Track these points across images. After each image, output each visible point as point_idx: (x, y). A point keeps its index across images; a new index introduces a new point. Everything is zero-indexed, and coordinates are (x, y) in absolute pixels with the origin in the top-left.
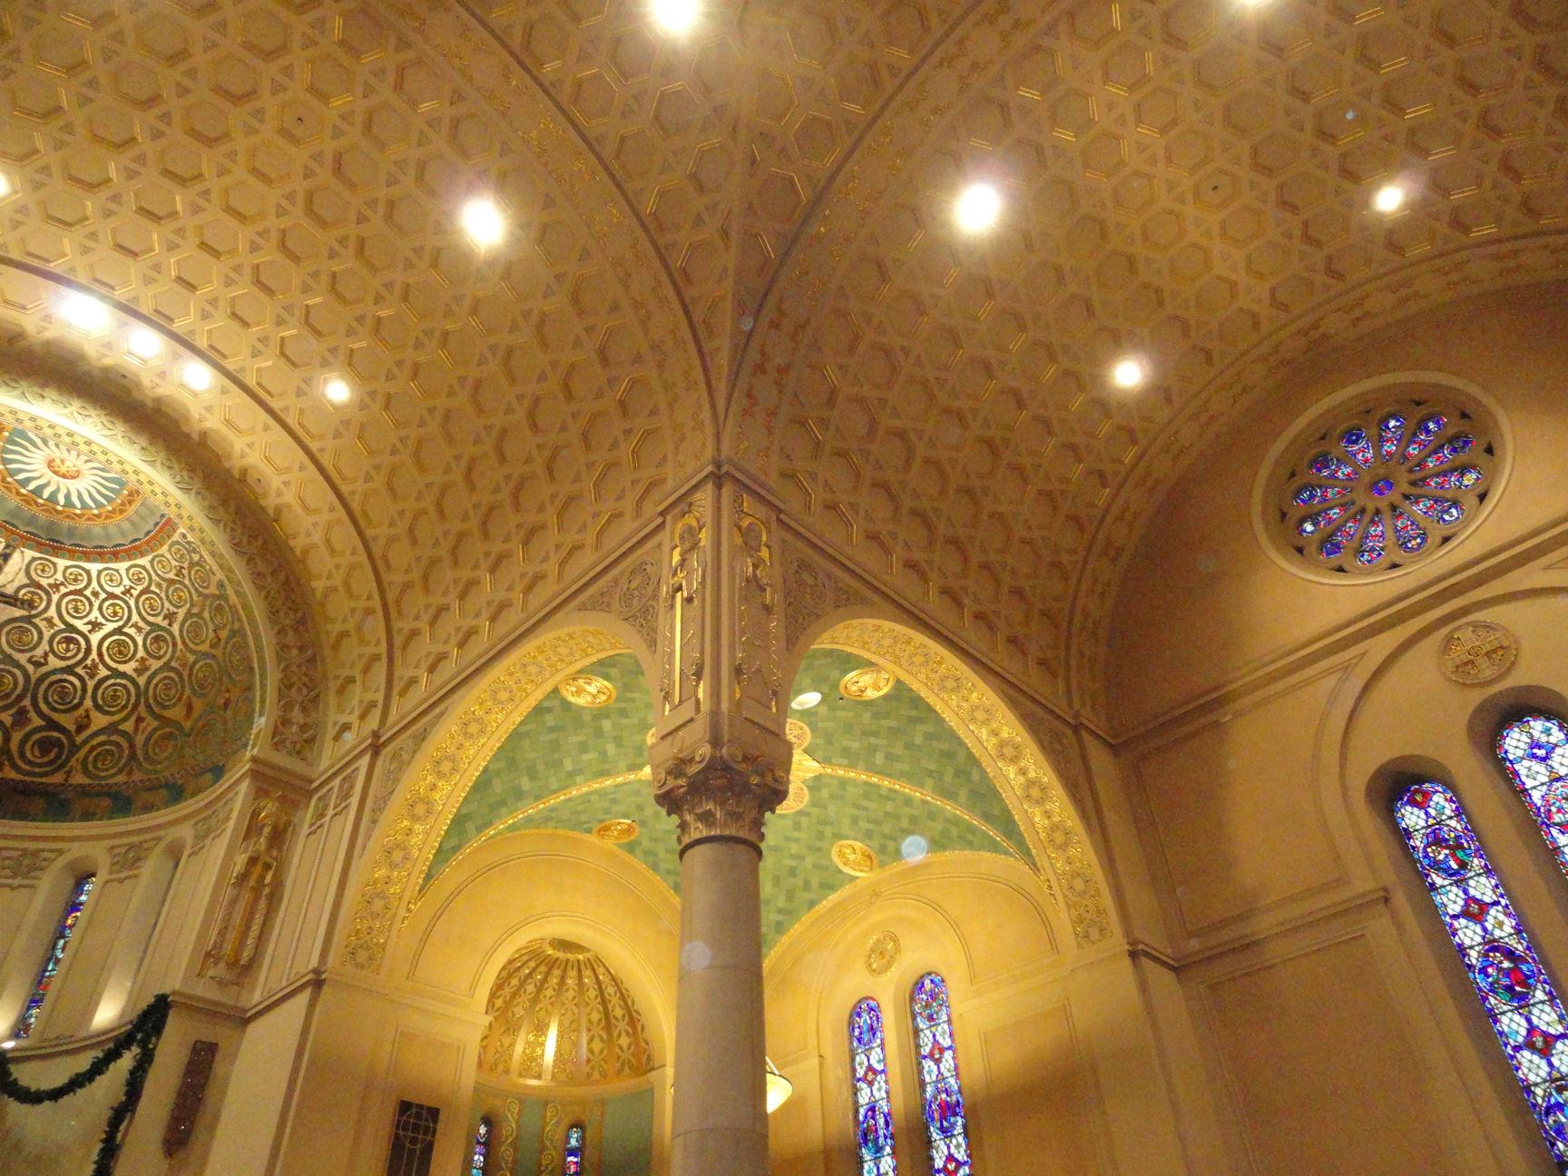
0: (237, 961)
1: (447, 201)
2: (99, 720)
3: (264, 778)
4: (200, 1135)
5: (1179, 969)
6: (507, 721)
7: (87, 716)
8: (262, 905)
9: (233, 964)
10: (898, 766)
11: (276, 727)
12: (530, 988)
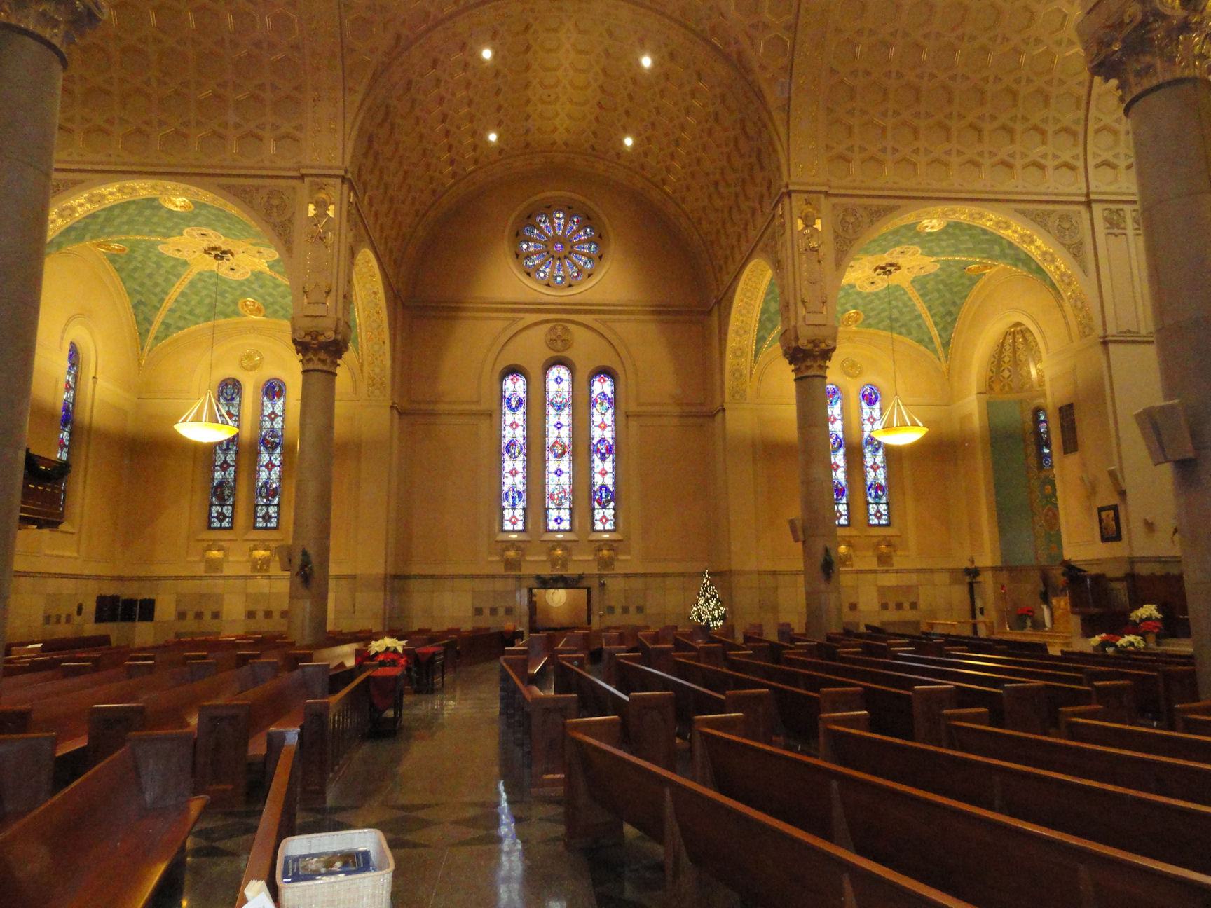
5: (400, 414)
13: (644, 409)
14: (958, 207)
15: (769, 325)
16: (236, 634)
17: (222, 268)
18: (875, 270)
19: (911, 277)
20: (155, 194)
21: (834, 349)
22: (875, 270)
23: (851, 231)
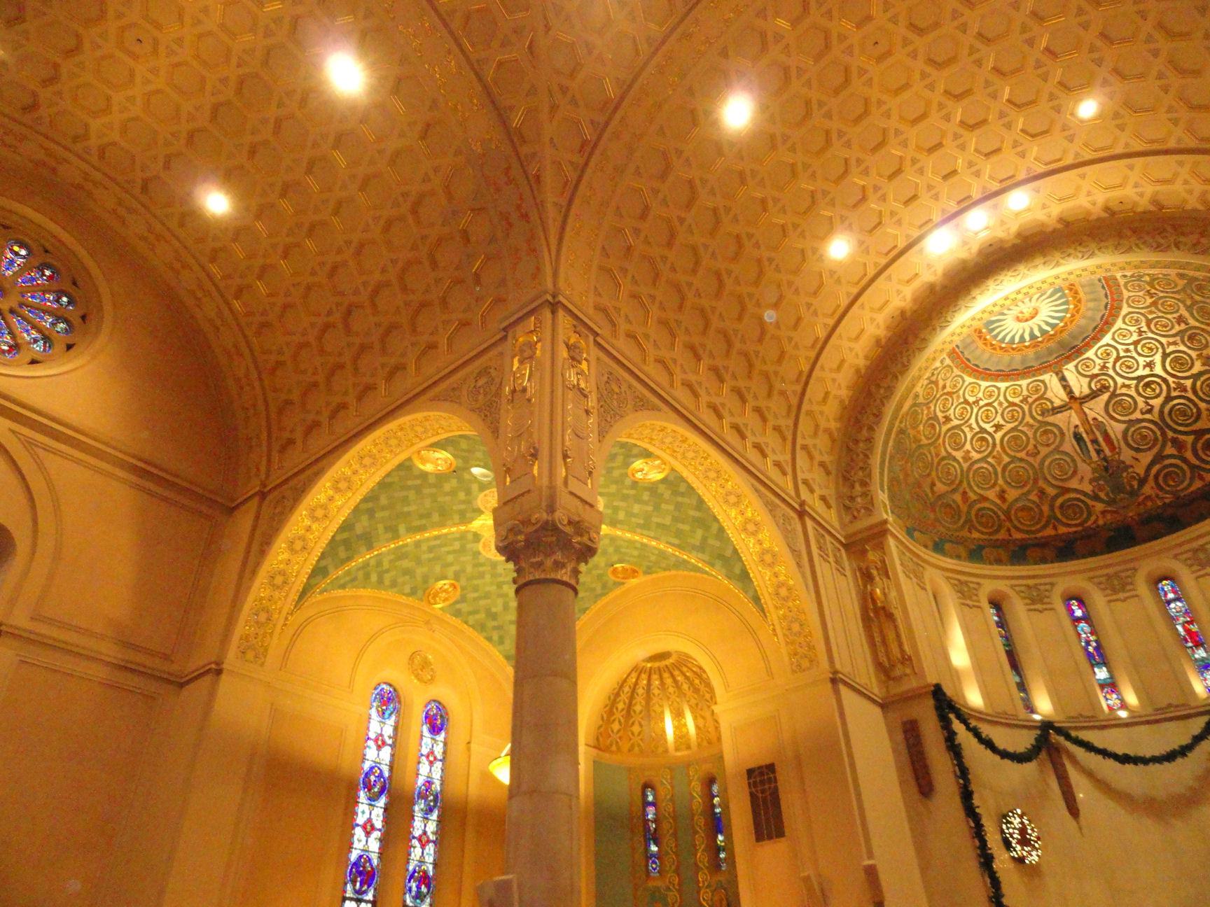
1: (1110, 470)
6: (369, 480)
13: (44, 629)
15: (342, 554)
16: (980, 876)
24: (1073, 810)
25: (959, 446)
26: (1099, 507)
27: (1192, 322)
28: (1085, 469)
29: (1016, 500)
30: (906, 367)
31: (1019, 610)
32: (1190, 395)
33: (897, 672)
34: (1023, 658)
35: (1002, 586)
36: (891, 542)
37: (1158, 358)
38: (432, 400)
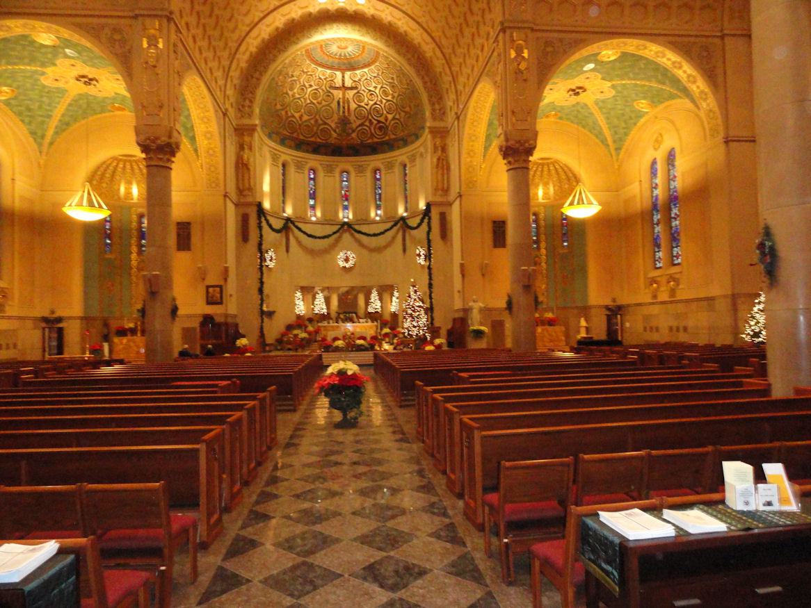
0: (443, 188)
1: (344, 121)
2: (390, 117)
3: (434, 131)
4: (448, 233)
7: (386, 117)
8: (445, 171)
9: (443, 190)
10: (640, 77)
11: (432, 114)
12: (538, 173)
14: (629, 41)
17: (91, 90)
18: (568, 92)
19: (593, 98)
20: (26, 31)
21: (535, 147)
22: (568, 92)
23: (549, 59)
24: (287, 251)
25: (292, 89)
26: (335, 135)
27: (395, 81)
28: (336, 117)
29: (306, 121)
30: (285, 49)
31: (292, 170)
32: (383, 106)
33: (246, 192)
34: (288, 191)
35: (288, 158)
36: (256, 134)
37: (379, 86)
38: (73, 24)
